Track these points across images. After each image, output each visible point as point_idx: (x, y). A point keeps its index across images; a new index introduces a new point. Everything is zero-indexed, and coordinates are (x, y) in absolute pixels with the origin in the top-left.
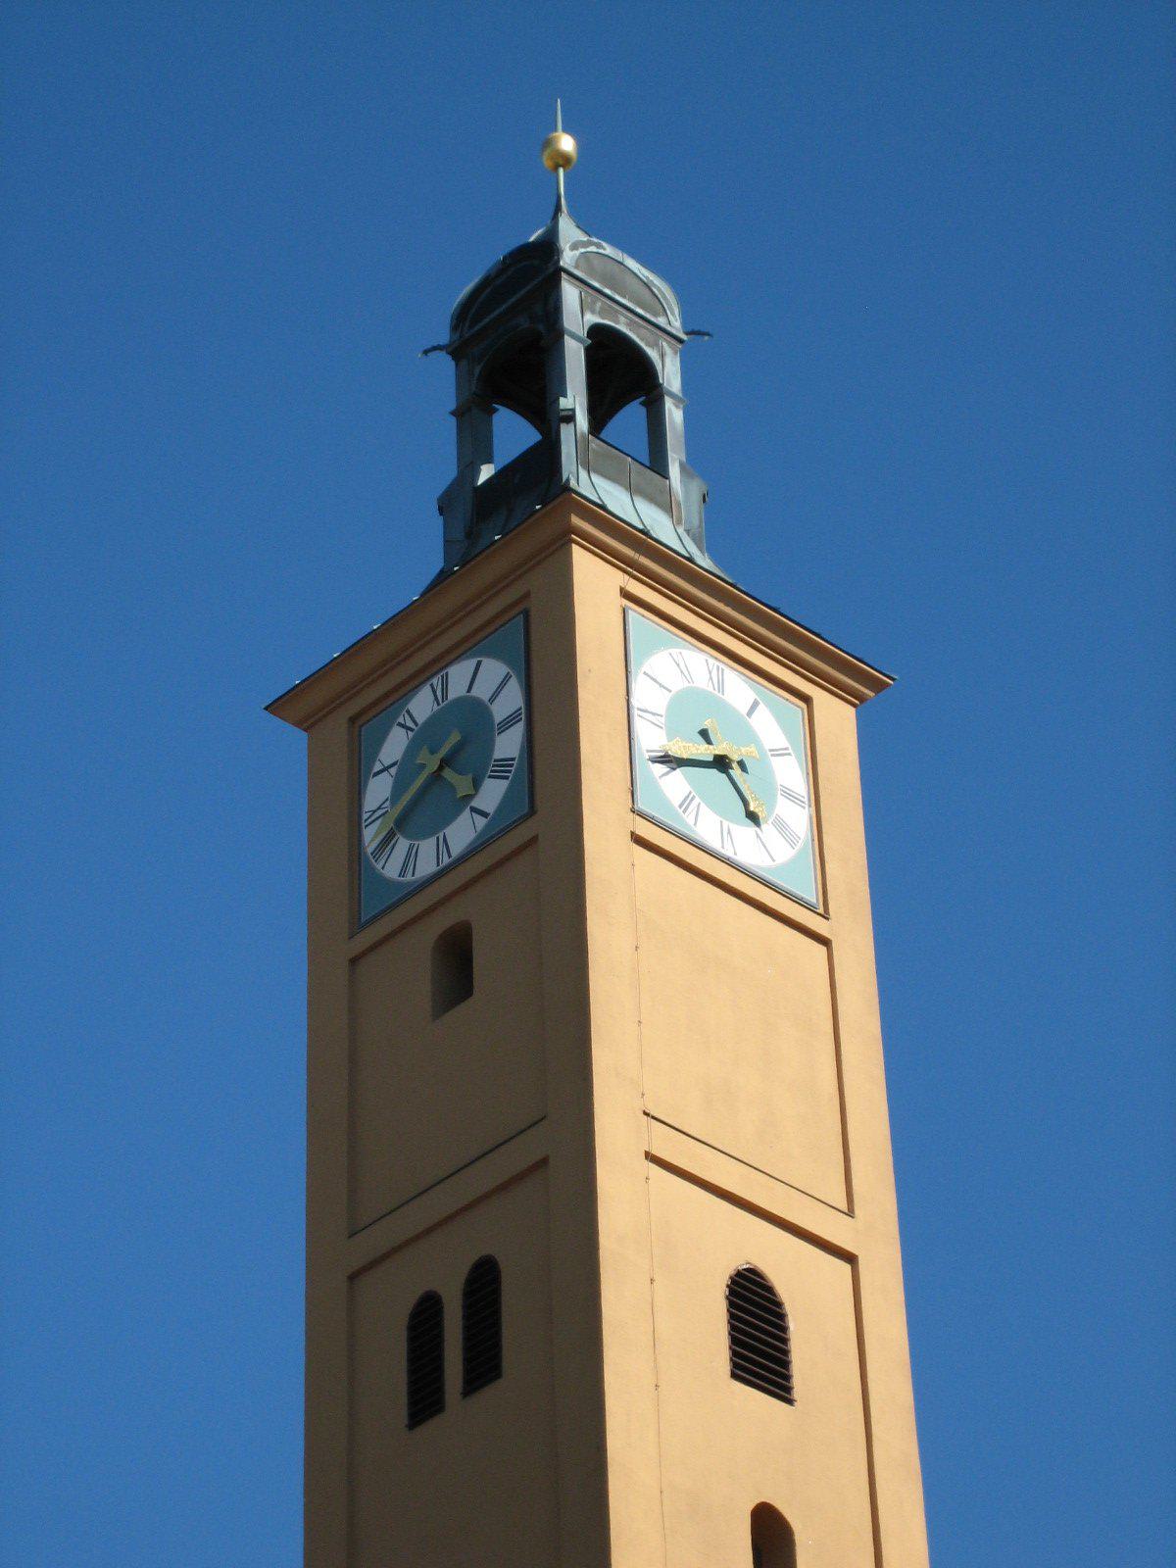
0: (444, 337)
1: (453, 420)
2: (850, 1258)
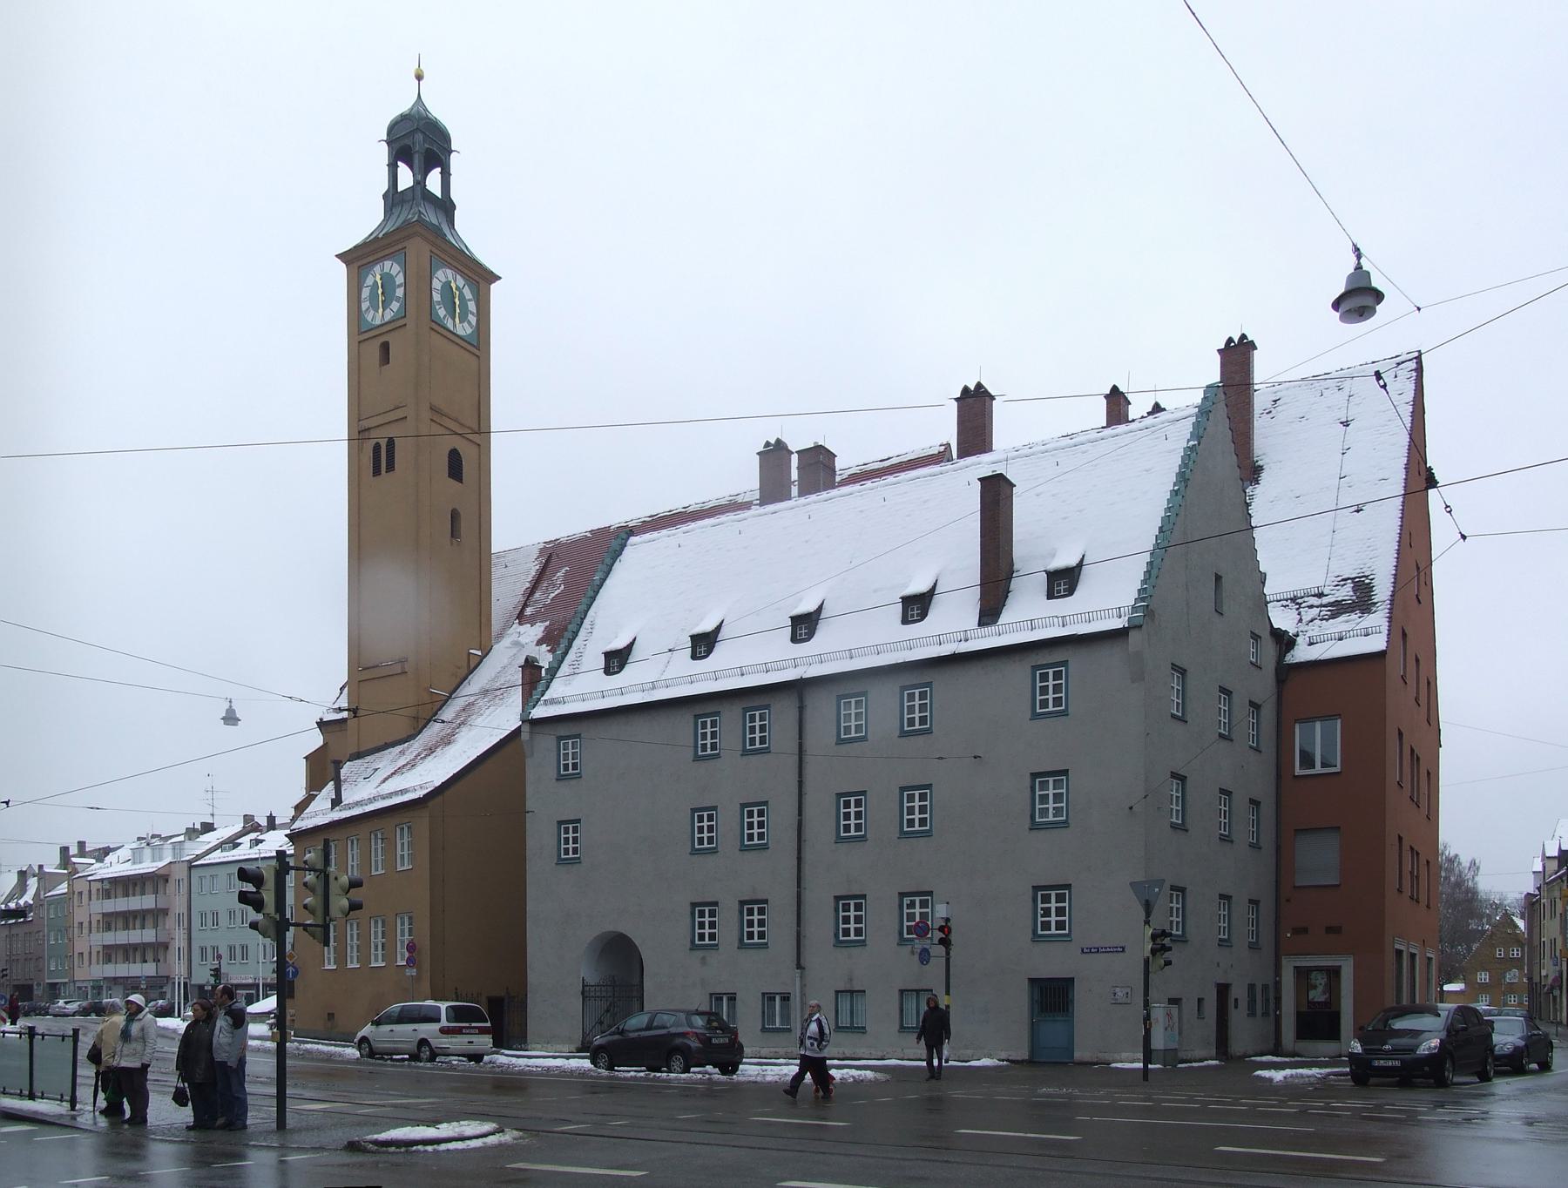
0: (385, 139)
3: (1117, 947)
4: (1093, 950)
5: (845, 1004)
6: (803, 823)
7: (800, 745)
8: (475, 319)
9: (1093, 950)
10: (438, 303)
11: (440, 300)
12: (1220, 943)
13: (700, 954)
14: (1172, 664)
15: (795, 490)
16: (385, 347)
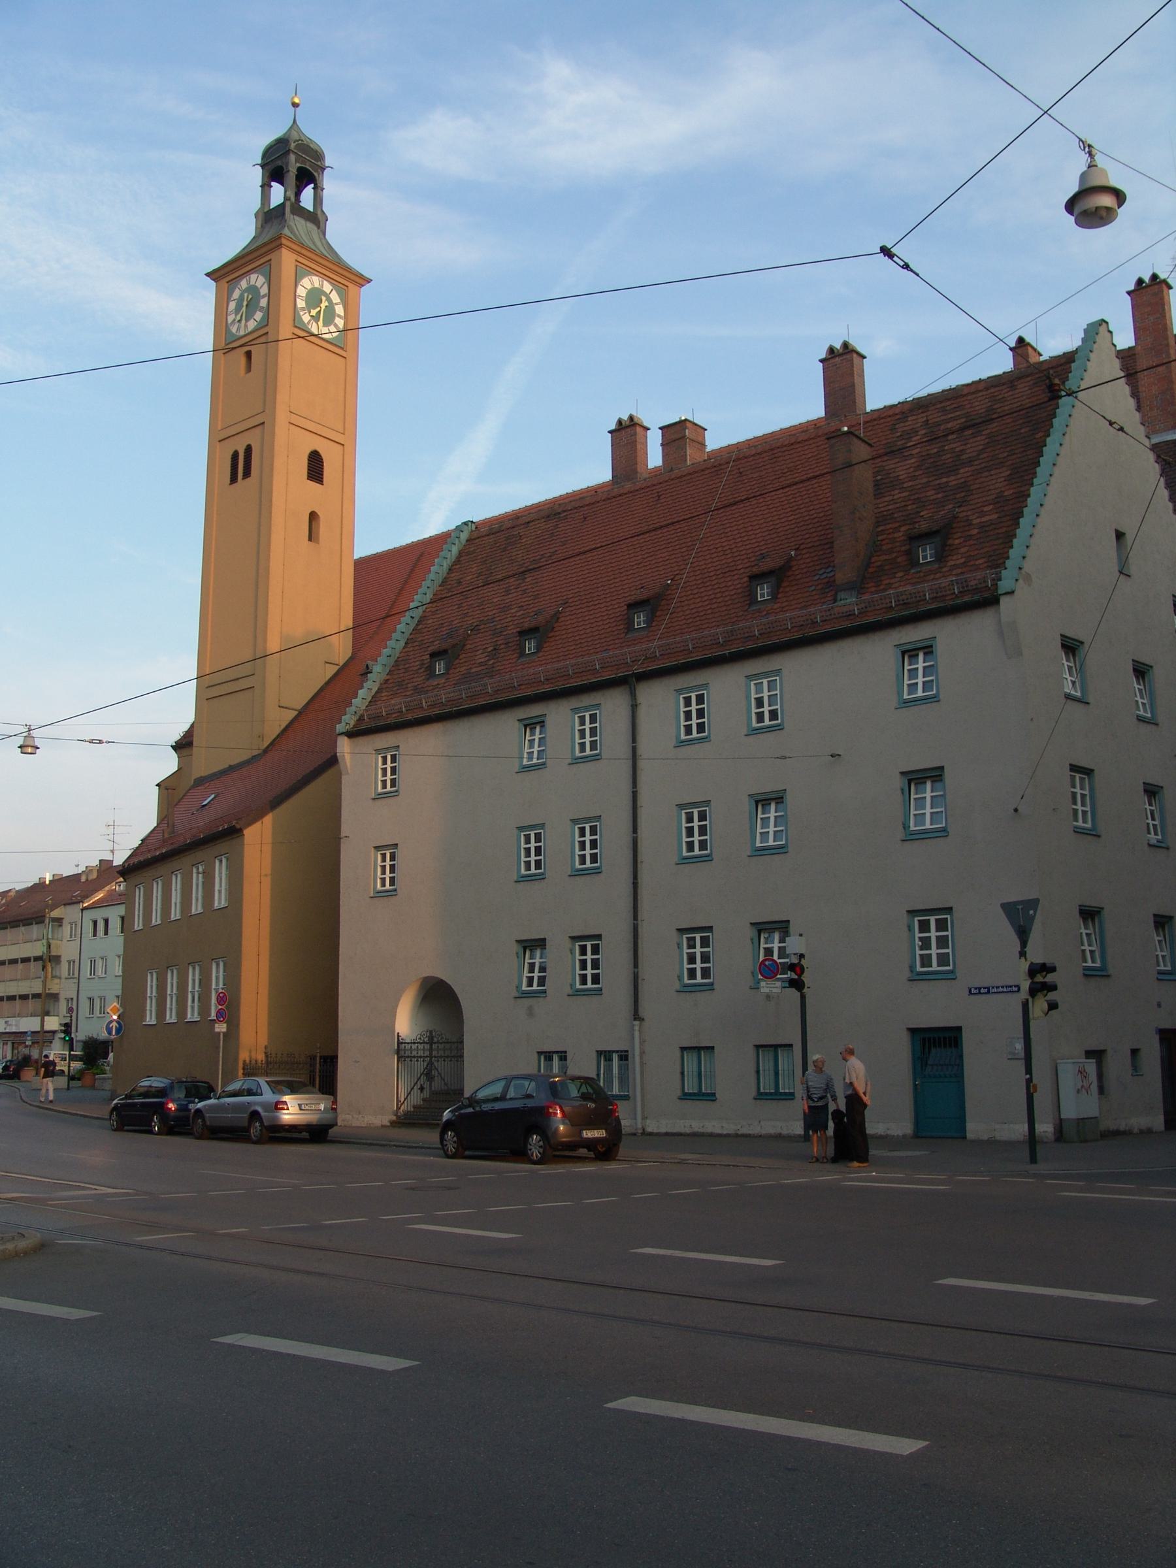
0: (259, 162)
1: (260, 188)
2: (343, 445)
3: (1011, 987)
4: (982, 991)
5: (766, 1064)
6: (639, 841)
7: (634, 750)
8: (343, 321)
9: (982, 991)
10: (303, 309)
11: (304, 306)
12: (1161, 977)
13: (526, 1002)
14: (1061, 635)
15: (1156, 440)
16: (249, 355)
